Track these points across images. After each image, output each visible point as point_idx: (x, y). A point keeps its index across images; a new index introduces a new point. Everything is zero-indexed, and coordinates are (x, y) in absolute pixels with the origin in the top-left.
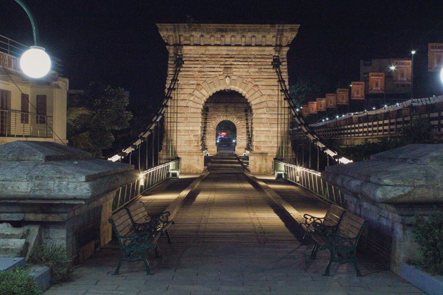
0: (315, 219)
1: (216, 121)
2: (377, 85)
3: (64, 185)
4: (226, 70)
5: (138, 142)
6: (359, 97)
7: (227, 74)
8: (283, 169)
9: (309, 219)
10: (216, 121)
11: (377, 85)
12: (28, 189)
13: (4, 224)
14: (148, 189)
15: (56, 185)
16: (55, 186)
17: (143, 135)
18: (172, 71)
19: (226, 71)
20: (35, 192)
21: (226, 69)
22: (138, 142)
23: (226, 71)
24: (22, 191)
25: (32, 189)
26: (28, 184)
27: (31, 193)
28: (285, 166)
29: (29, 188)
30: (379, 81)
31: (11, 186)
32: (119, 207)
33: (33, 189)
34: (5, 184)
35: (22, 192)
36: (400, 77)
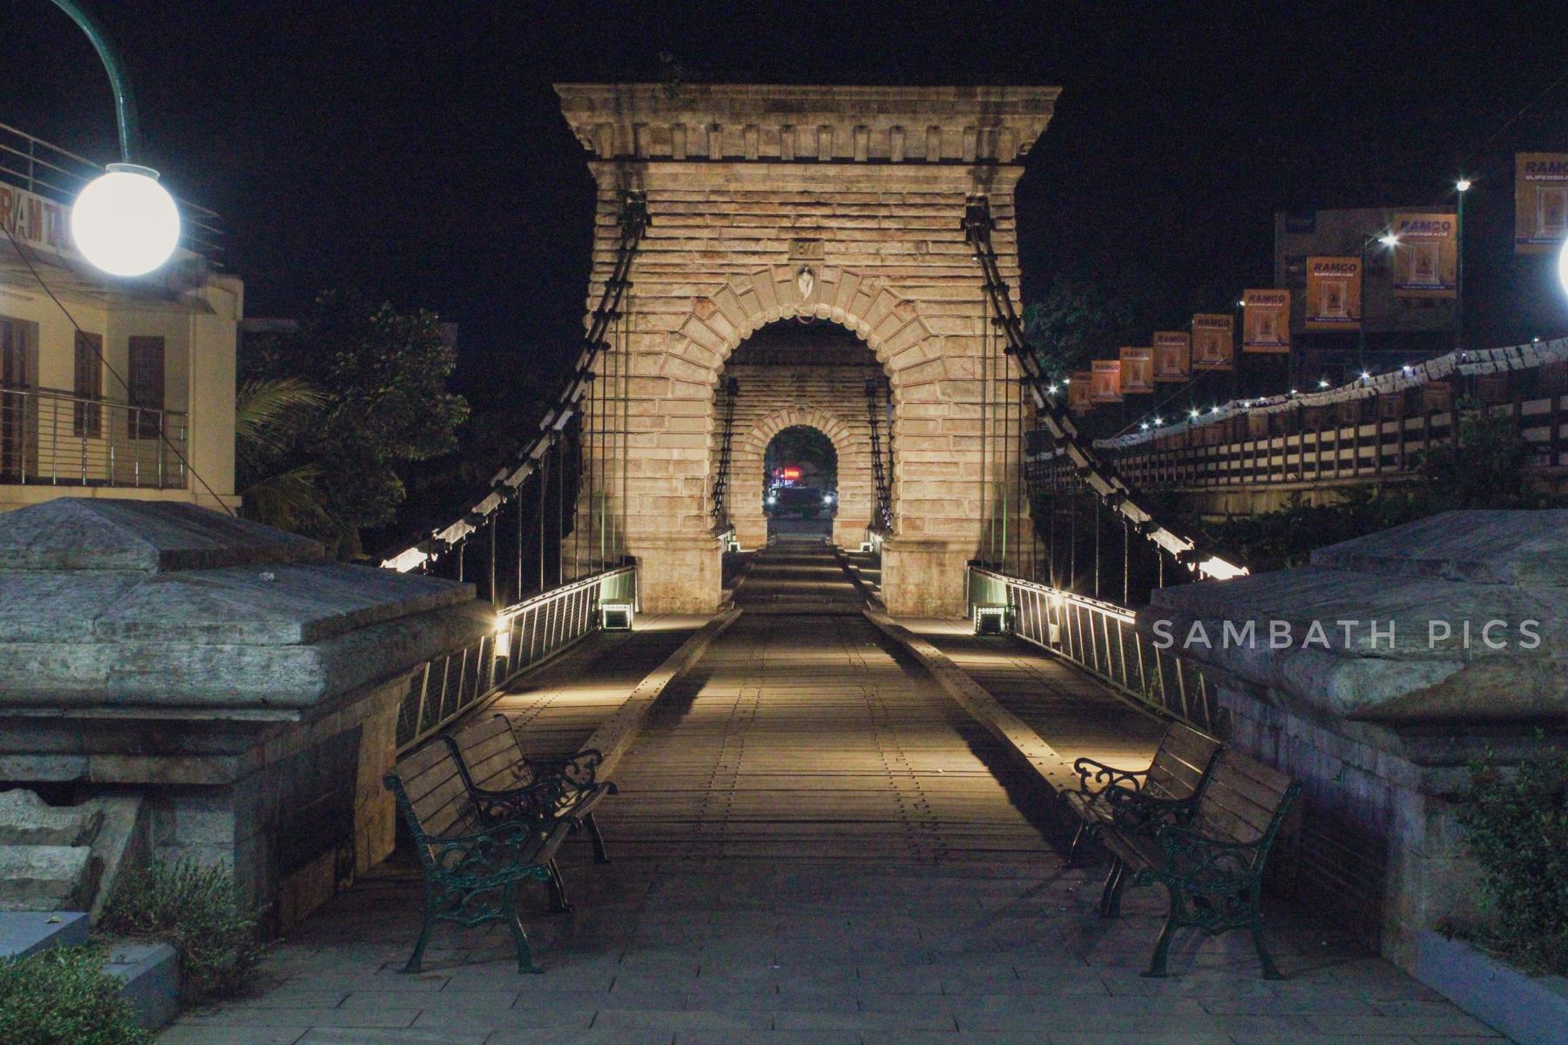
0: (1116, 776)
1: (766, 429)
2: (1334, 300)
3: (225, 655)
4: (801, 247)
5: (489, 505)
6: (1270, 344)
7: (802, 262)
8: (1002, 598)
9: (1094, 776)
10: (766, 429)
11: (1334, 300)
12: (98, 670)
13: (15, 795)
14: (524, 670)
15: (198, 654)
16: (196, 659)
17: (508, 478)
18: (608, 251)
19: (802, 250)
20: (122, 679)
21: (801, 244)
22: (489, 505)
23: (802, 250)
24: (78, 676)
25: (112, 668)
26: (99, 651)
27: (111, 683)
28: (1008, 588)
29: (102, 665)
30: (1343, 285)
31: (39, 658)
32: (420, 733)
33: (117, 668)
34: (16, 652)
35: (76, 680)
36: (1418, 272)
